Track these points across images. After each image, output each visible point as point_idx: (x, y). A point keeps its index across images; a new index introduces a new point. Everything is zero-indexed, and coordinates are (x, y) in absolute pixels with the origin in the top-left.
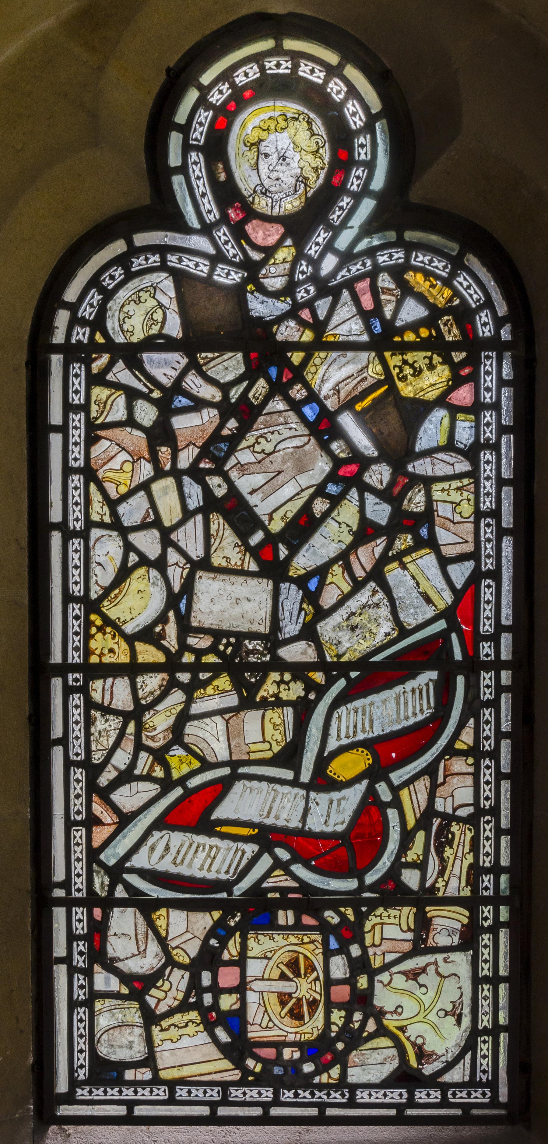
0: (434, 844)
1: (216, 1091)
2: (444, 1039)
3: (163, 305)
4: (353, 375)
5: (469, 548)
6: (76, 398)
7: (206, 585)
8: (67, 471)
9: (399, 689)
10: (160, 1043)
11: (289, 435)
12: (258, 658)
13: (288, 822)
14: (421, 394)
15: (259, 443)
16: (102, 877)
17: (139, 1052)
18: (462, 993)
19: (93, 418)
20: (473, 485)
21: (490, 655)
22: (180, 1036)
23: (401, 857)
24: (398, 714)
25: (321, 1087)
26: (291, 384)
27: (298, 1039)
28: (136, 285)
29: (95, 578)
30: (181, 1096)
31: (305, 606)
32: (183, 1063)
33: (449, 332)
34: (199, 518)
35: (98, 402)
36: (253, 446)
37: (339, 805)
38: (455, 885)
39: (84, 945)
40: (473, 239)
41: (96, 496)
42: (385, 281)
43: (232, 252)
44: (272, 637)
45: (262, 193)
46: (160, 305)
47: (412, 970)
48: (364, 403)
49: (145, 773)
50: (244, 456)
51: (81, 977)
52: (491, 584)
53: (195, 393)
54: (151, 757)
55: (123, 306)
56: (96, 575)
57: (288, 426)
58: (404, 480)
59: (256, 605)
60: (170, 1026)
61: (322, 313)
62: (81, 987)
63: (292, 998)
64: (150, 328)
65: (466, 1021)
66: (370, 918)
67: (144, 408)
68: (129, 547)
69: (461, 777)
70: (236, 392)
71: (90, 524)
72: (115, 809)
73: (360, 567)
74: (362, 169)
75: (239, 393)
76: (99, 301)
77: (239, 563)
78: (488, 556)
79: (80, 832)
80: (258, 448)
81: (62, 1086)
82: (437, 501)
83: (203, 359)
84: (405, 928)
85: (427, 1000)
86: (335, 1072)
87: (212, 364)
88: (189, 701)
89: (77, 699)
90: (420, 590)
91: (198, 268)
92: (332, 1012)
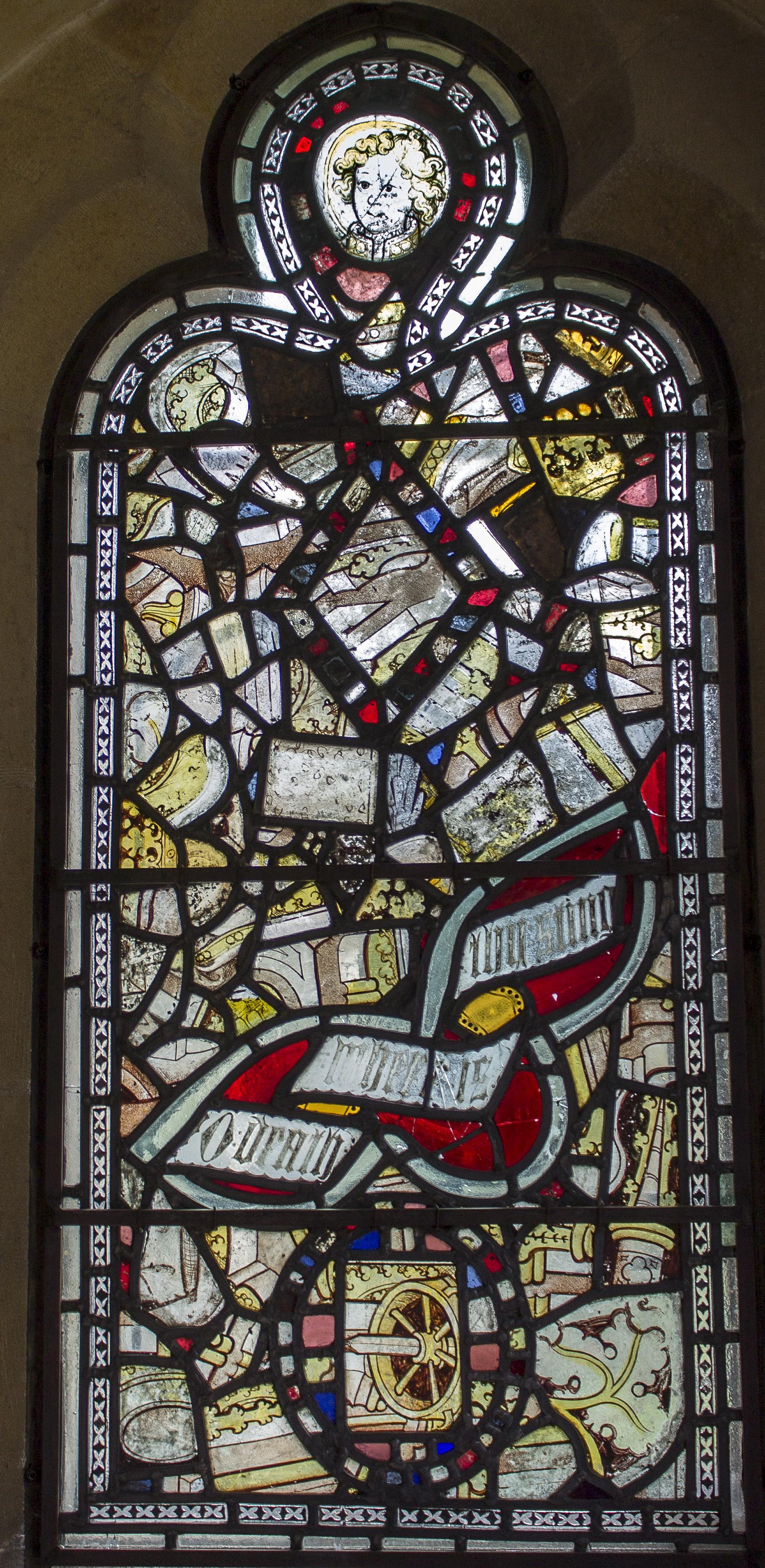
0: (619, 1129)
1: (300, 1510)
2: (642, 1429)
3: (225, 383)
4: (487, 469)
5: (656, 701)
6: (106, 508)
7: (287, 762)
8: (93, 606)
9: (561, 901)
10: (216, 1434)
11: (398, 552)
12: (358, 860)
13: (403, 1095)
14: (583, 492)
15: (357, 564)
16: (134, 1180)
17: (184, 1449)
18: (668, 1358)
19: (130, 534)
20: (658, 615)
21: (692, 852)
22: (246, 1423)
23: (571, 1148)
24: (560, 937)
25: (459, 1505)
26: (401, 483)
27: (422, 1428)
28: (190, 357)
29: (129, 751)
30: (247, 1518)
31: (424, 786)
32: (250, 1466)
33: (620, 408)
34: (275, 667)
35: (136, 513)
36: (349, 567)
37: (477, 1070)
38: (652, 1190)
39: (106, 1283)
40: (647, 283)
41: (132, 639)
42: (529, 343)
43: (319, 311)
44: (377, 830)
45: (359, 233)
46: (222, 383)
47: (592, 1321)
48: (503, 507)
49: (197, 1024)
50: (338, 582)
51: (101, 1332)
52: (690, 750)
53: (270, 498)
54: (206, 1002)
55: (171, 385)
56: (132, 748)
57: (397, 540)
58: (560, 610)
59: (355, 785)
60: (231, 1407)
61: (442, 389)
62: (101, 1347)
63: (414, 1364)
64: (208, 413)
65: (676, 1402)
66: (527, 1240)
67: (199, 520)
68: (177, 708)
69: (654, 1028)
70: (326, 496)
71: (123, 677)
72: (153, 1077)
73: (500, 730)
74: (495, 198)
75: (330, 496)
76: (138, 379)
77: (331, 727)
78: (684, 712)
79: (103, 1113)
80: (355, 571)
81: (69, 1503)
82: (608, 637)
83: (280, 452)
84: (579, 1256)
85: (617, 1368)
86: (480, 1481)
87: (292, 460)
88: (261, 922)
89: (102, 920)
90: (587, 761)
91: (274, 334)
92: (474, 1387)
